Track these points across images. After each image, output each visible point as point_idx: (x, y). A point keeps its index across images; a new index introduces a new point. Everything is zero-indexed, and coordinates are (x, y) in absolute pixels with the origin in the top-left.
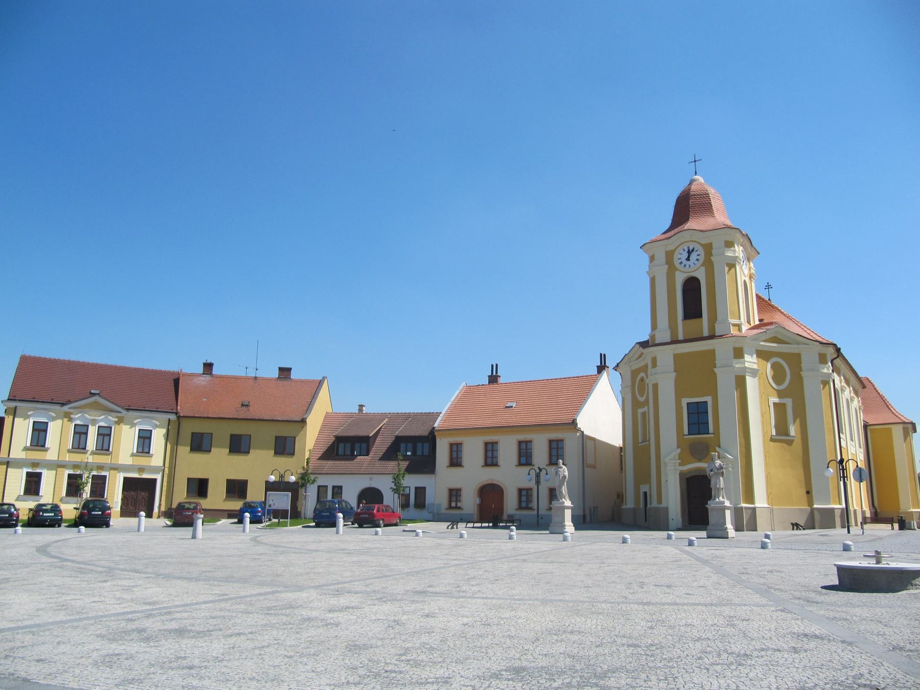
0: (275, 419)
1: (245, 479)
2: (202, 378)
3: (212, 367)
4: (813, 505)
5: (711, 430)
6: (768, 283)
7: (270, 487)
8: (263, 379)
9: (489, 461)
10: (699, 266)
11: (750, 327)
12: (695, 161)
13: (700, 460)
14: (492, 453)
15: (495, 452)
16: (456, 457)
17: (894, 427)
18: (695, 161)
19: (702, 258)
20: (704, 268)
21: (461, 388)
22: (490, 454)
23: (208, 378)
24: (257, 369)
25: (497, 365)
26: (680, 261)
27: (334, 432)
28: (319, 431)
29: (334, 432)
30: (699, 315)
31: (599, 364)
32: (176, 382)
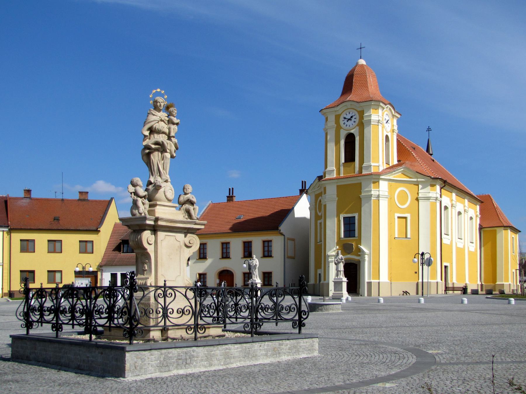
0: (78, 229)
1: (120, 275)
2: (24, 201)
3: (31, 192)
4: (496, 282)
5: (356, 235)
6: (429, 127)
7: (79, 274)
8: (68, 200)
9: (266, 254)
10: (355, 126)
11: (388, 166)
12: (361, 48)
13: (349, 254)
14: (268, 248)
15: (205, 250)
16: (225, 252)
17: (397, 237)
18: (361, 48)
19: (357, 121)
20: (358, 127)
21: (208, 205)
22: (266, 249)
23: (28, 200)
24: (62, 193)
25: (233, 189)
26: (345, 125)
27: (121, 236)
28: (110, 236)
29: (121, 236)
30: (353, 160)
31: (301, 188)
32: (6, 202)
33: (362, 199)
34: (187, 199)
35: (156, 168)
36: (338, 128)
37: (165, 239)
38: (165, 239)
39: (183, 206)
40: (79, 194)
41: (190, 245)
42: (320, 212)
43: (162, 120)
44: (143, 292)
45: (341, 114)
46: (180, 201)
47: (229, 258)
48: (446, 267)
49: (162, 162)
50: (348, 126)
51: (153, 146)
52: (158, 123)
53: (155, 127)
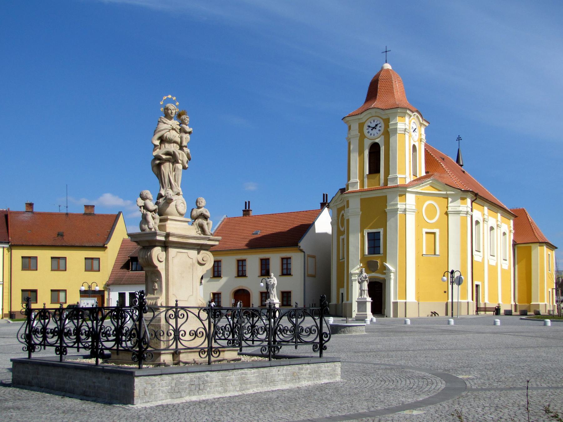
0: (84, 245)
2: (26, 215)
3: (33, 206)
5: (382, 251)
6: (459, 136)
7: (84, 294)
8: (73, 215)
9: (285, 272)
10: (380, 134)
11: (415, 178)
12: (386, 52)
13: (373, 272)
14: (287, 265)
15: (219, 268)
16: (241, 270)
17: (425, 254)
18: (386, 52)
19: (382, 129)
20: (383, 136)
21: (222, 219)
22: (285, 266)
23: (30, 215)
24: (67, 207)
25: (249, 202)
26: (370, 134)
27: (129, 253)
28: (118, 252)
29: (129, 253)
30: (378, 171)
31: (322, 202)
32: (6, 216)
33: (388, 213)
34: (200, 213)
35: (167, 180)
36: (362, 137)
37: (176, 256)
38: (176, 256)
39: (196, 220)
40: (85, 207)
41: (203, 262)
42: (342, 227)
43: (173, 129)
44: (153, 313)
45: (365, 122)
46: (193, 216)
47: (245, 276)
48: (477, 286)
49: (174, 173)
50: (372, 135)
51: (164, 157)
52: (169, 131)
53: (166, 136)
